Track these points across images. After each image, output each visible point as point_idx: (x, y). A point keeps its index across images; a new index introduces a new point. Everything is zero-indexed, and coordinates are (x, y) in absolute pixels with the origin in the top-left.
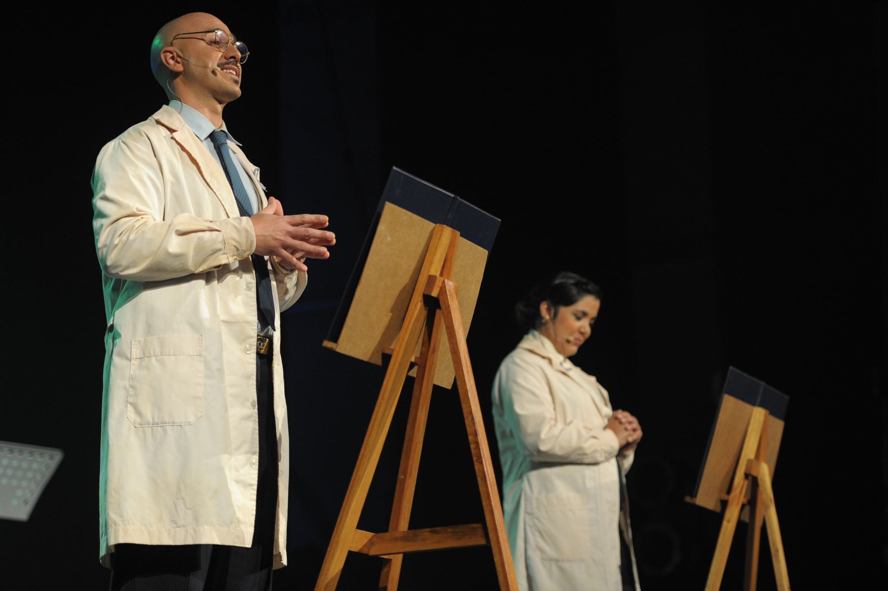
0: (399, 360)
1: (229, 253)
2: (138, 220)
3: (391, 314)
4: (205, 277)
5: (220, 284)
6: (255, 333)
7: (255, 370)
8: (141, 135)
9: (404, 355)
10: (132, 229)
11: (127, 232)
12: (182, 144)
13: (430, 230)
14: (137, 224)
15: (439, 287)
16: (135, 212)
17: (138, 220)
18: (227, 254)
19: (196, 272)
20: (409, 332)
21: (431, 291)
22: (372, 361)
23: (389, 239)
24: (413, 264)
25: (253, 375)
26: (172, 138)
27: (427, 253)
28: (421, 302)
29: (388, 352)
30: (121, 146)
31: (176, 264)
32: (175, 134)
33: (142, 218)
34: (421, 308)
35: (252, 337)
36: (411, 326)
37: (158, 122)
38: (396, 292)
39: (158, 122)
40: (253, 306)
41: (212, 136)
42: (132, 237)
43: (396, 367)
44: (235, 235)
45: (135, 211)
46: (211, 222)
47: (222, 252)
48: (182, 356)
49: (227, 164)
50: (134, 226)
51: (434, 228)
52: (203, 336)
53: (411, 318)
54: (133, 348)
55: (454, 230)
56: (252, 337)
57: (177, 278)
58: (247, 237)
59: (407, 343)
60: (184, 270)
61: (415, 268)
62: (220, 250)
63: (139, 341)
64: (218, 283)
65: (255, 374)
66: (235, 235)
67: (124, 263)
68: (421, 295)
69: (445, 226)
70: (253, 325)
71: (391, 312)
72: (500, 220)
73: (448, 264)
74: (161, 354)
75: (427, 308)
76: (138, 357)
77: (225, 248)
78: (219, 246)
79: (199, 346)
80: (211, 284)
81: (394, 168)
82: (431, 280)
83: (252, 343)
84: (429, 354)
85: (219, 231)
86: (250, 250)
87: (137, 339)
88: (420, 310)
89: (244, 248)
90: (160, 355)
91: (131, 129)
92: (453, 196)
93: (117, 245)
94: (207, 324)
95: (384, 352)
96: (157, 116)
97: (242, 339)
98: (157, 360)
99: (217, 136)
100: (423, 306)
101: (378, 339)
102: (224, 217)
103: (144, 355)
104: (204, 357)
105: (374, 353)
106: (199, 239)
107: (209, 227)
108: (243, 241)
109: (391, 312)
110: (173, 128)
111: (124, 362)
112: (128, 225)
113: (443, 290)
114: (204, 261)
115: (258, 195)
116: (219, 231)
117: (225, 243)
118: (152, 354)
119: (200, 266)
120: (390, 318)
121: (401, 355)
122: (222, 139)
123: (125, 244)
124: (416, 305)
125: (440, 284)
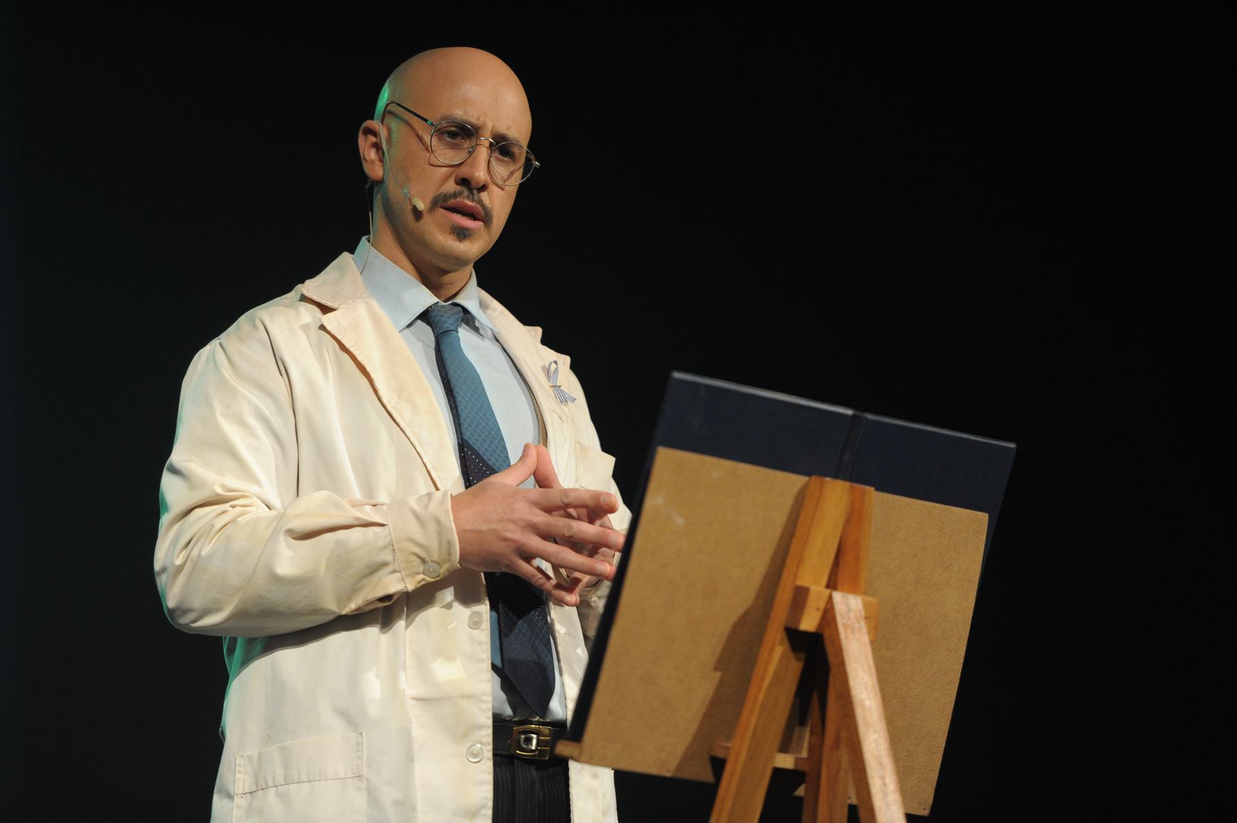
0: (739, 768)
1: (404, 570)
2: (224, 512)
3: (718, 675)
4: (380, 620)
5: (384, 633)
6: (488, 718)
7: (490, 795)
8: (255, 326)
9: (750, 758)
10: (211, 530)
11: (198, 541)
12: (339, 337)
13: (795, 490)
14: (219, 523)
15: (818, 609)
16: (218, 495)
17: (224, 512)
18: (400, 572)
19: (344, 613)
20: (757, 708)
21: (799, 620)
22: (687, 775)
23: (680, 521)
24: (759, 568)
25: (484, 807)
26: (322, 327)
27: (794, 540)
28: (781, 643)
29: (719, 754)
30: (215, 363)
31: (300, 599)
32: (329, 320)
33: (233, 507)
34: (783, 656)
35: (481, 727)
36: (761, 697)
37: (304, 299)
38: (724, 626)
39: (304, 299)
40: (483, 661)
41: (425, 316)
42: (204, 553)
43: (734, 785)
44: (415, 531)
45: (219, 491)
46: (374, 506)
47: (390, 568)
48: (323, 782)
49: (451, 372)
50: (212, 526)
51: (804, 490)
52: (364, 734)
53: (762, 679)
54: (239, 772)
55: (855, 485)
56: (481, 727)
57: (324, 624)
58: (440, 534)
59: (754, 734)
60: (316, 611)
61: (767, 573)
62: (385, 564)
63: (250, 758)
64: (407, 627)
65: (490, 804)
66: (415, 531)
67: (197, 602)
68: (781, 629)
69: (827, 479)
70: (483, 702)
71: (716, 668)
72: (1012, 445)
73: (848, 558)
74: (285, 781)
75: (803, 656)
76: (248, 791)
77: (394, 560)
78: (387, 556)
79: (358, 757)
80: (393, 629)
81: (677, 375)
82: (801, 595)
83: (484, 740)
84: (826, 749)
85: (383, 525)
86: (449, 560)
87: (245, 754)
88: (780, 661)
89: (436, 557)
90: (283, 783)
91: (243, 319)
92: (849, 412)
93: (181, 567)
94: (373, 710)
95: (713, 753)
96: (309, 287)
97: (460, 732)
98: (278, 795)
99: (436, 316)
100: (789, 652)
101: (693, 728)
102: (424, 487)
103: (257, 786)
104: (367, 780)
105: (686, 758)
106: (338, 543)
107: (358, 519)
108: (433, 543)
109: (716, 668)
110: (329, 304)
111: (225, 802)
112: (202, 522)
113: (828, 615)
114: (355, 590)
115: (540, 419)
116: (383, 525)
117: (394, 550)
118: (270, 784)
119: (349, 599)
120: (716, 682)
121: (742, 758)
122: (446, 322)
123: (196, 564)
124: (771, 651)
125: (822, 605)
